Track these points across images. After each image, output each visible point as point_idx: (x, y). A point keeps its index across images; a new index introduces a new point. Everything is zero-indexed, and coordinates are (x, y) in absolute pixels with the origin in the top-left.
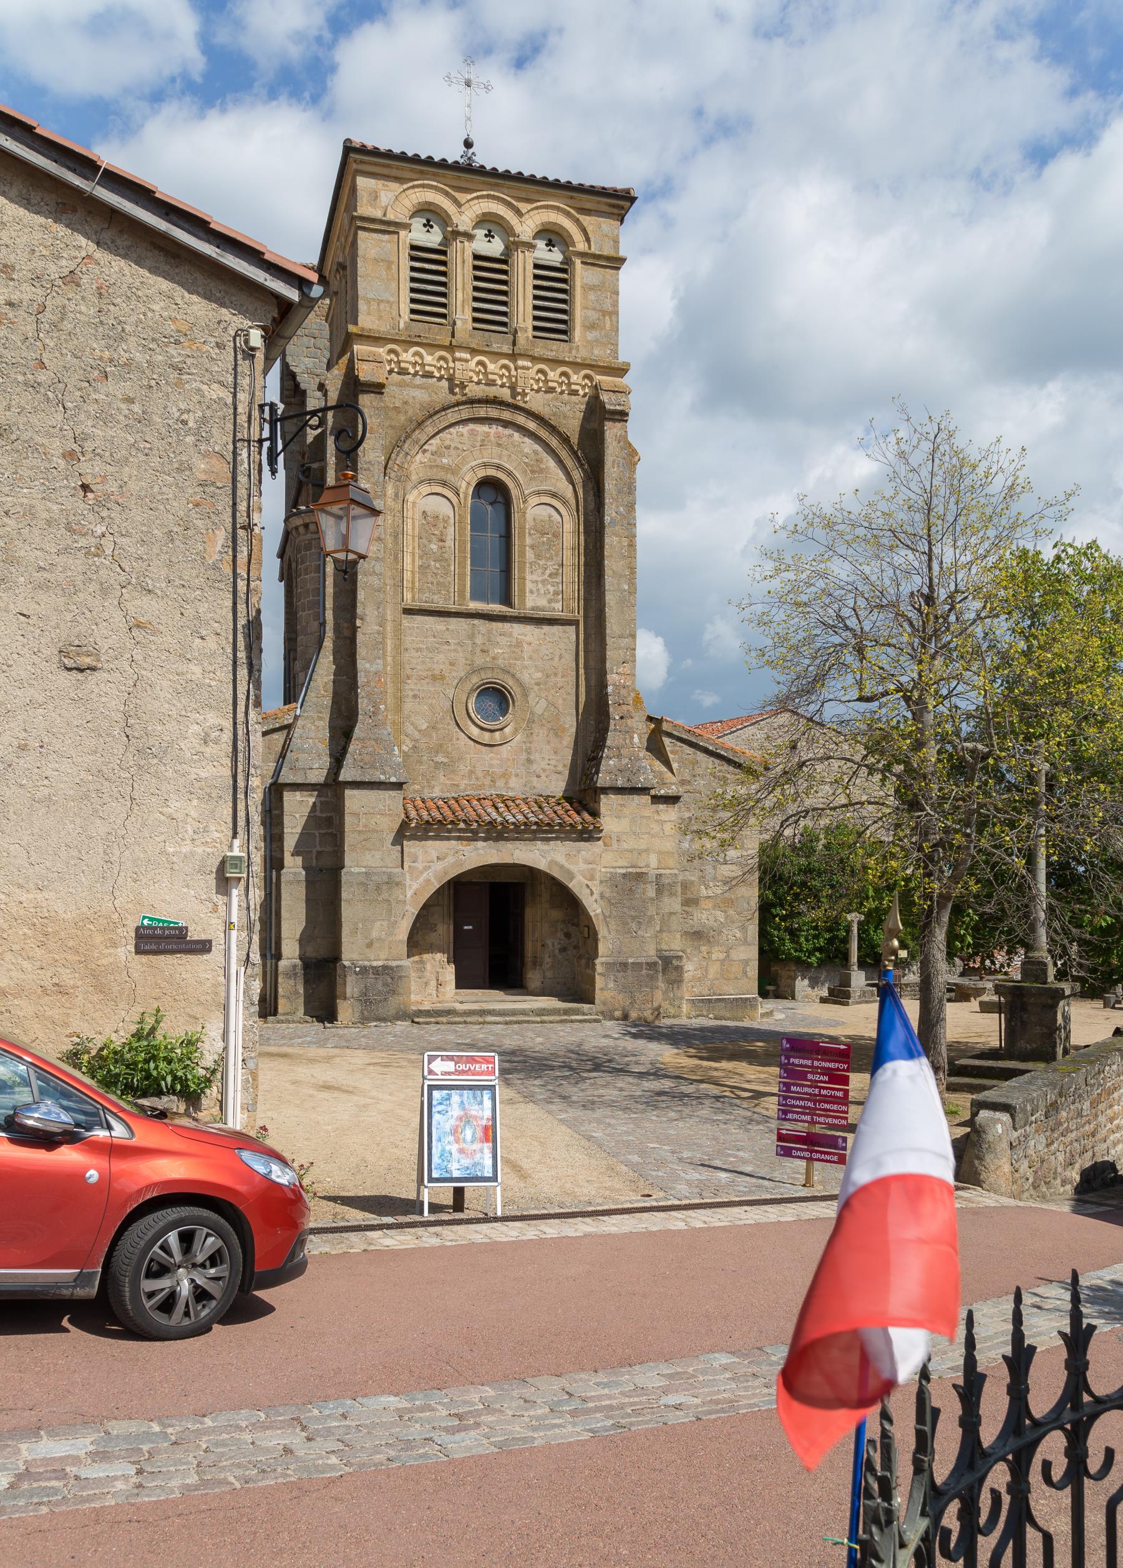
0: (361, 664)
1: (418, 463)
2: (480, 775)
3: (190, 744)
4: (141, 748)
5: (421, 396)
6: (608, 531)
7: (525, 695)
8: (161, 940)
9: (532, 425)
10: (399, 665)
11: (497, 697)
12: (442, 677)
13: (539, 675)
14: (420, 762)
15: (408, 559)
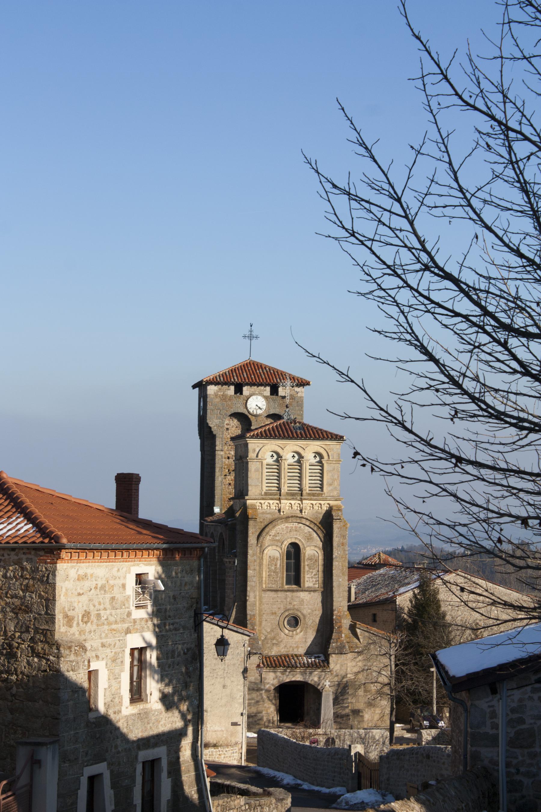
0: (249, 612)
1: (267, 539)
2: (289, 647)
3: (238, 697)
4: (232, 698)
5: (269, 516)
6: (334, 560)
7: (305, 618)
8: (234, 724)
9: (308, 523)
10: (260, 610)
11: (295, 622)
12: (275, 613)
13: (310, 611)
14: (268, 643)
15: (264, 573)
